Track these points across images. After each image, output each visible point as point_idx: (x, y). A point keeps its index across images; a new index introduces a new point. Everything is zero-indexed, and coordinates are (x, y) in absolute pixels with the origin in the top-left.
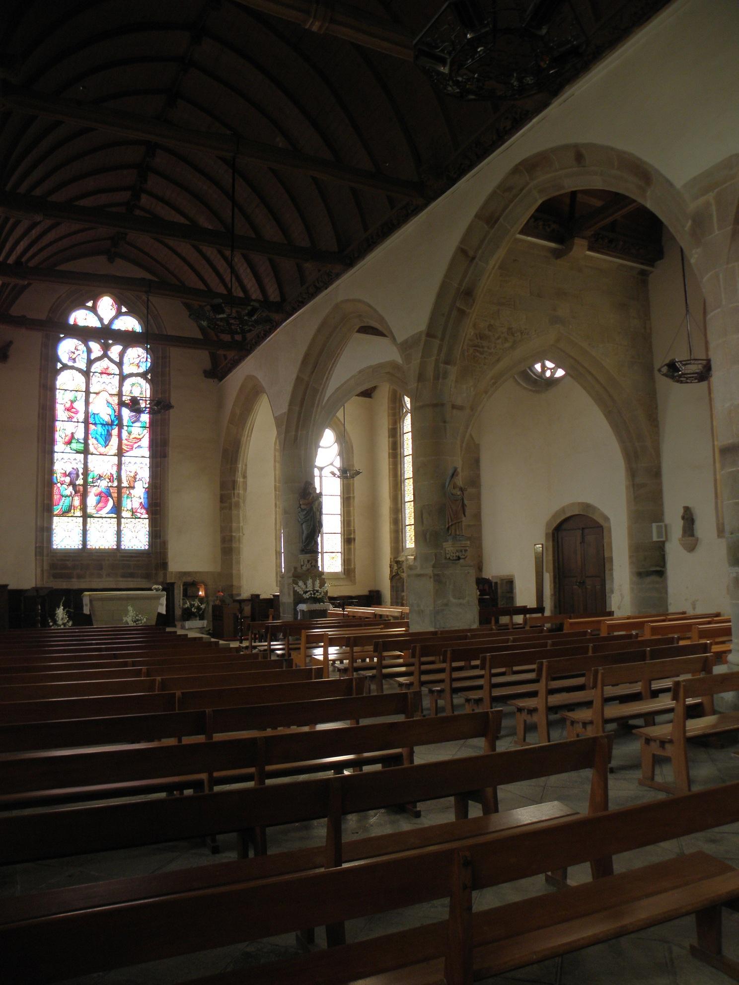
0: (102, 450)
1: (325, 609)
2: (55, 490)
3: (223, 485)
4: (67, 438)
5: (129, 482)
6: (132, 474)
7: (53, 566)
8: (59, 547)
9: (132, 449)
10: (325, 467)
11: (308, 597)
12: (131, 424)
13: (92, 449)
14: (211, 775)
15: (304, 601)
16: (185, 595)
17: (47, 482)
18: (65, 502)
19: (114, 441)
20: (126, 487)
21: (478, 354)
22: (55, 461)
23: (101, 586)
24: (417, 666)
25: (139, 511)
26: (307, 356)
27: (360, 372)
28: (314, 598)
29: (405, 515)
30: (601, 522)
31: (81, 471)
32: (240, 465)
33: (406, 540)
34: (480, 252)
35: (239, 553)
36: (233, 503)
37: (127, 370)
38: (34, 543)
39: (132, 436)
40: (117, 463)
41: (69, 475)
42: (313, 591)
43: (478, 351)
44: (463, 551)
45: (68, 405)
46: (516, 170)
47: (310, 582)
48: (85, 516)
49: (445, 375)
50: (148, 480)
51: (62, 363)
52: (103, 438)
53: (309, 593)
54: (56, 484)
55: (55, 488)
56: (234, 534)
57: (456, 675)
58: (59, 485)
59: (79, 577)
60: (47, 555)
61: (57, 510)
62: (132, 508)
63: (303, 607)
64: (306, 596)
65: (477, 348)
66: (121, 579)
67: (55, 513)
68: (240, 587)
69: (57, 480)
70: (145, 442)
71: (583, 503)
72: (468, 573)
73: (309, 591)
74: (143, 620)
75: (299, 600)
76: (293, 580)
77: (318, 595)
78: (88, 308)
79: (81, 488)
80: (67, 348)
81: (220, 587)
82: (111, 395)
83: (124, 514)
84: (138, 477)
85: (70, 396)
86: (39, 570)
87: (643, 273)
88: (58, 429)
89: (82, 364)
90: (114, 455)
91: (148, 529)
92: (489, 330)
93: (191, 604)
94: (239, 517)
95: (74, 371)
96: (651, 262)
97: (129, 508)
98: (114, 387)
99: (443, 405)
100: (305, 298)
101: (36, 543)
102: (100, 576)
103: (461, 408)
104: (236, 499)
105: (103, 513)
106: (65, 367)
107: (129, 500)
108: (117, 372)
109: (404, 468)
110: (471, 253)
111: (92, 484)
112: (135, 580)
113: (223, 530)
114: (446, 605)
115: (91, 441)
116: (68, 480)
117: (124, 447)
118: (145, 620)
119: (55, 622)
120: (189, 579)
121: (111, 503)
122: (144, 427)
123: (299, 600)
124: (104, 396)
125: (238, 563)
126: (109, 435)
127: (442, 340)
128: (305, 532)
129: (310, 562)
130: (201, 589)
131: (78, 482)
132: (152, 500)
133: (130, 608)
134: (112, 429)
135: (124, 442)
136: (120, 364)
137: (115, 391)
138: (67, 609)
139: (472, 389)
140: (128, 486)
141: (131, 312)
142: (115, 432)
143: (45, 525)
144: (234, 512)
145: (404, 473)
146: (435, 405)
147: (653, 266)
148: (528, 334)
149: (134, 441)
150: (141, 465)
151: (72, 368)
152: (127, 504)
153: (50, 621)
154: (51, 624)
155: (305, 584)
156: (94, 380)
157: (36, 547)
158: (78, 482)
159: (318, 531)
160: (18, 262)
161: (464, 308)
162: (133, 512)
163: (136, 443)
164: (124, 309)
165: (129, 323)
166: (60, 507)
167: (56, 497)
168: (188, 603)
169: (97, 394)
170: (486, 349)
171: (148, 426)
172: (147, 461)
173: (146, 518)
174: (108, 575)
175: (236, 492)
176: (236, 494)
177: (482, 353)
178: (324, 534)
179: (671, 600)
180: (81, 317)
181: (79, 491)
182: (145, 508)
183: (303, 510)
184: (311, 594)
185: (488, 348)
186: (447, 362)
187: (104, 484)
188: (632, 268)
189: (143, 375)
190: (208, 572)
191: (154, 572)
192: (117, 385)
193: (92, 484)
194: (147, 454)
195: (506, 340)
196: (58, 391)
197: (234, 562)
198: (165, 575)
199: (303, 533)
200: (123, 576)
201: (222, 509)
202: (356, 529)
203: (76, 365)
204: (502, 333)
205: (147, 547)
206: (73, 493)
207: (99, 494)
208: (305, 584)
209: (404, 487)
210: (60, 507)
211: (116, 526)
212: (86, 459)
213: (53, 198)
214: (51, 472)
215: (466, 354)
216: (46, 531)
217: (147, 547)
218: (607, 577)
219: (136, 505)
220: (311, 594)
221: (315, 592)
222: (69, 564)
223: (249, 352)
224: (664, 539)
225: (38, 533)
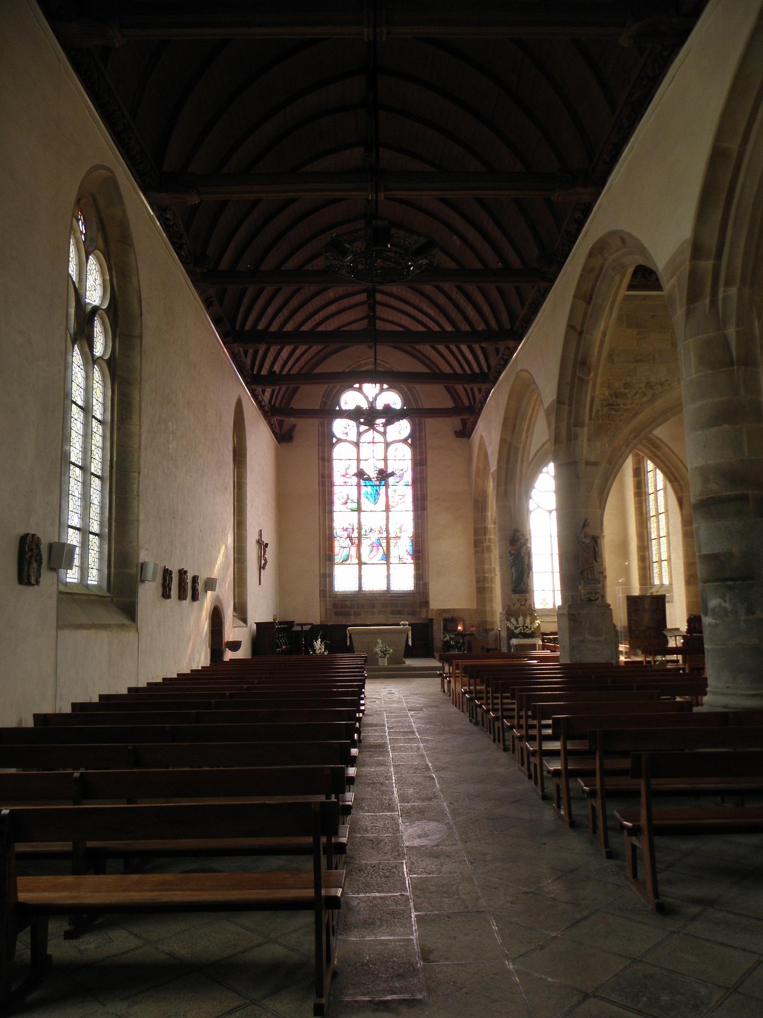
0: (373, 507)
3: (476, 532)
7: (335, 606)
11: (518, 632)
12: (396, 484)
13: (363, 508)
15: (516, 636)
16: (446, 629)
17: (328, 538)
21: (613, 412)
28: (524, 633)
29: (652, 552)
31: (356, 526)
32: (489, 513)
33: (654, 577)
34: (585, 326)
35: (492, 591)
38: (318, 586)
41: (346, 530)
42: (523, 627)
43: (612, 409)
44: (593, 593)
46: (591, 255)
47: (521, 619)
48: (360, 563)
53: (519, 629)
56: (486, 575)
57: (505, 701)
60: (330, 597)
61: (337, 559)
63: (514, 641)
64: (517, 631)
73: (519, 627)
74: (390, 650)
75: (511, 635)
76: (506, 618)
78: (356, 389)
79: (357, 541)
80: (341, 427)
81: (476, 622)
86: (323, 610)
92: (625, 388)
93: (450, 638)
95: (347, 444)
100: (500, 369)
101: (320, 587)
102: (373, 613)
104: (488, 544)
106: (339, 440)
107: (396, 547)
109: (649, 505)
110: (578, 328)
111: (365, 536)
112: (402, 616)
114: (582, 641)
116: (345, 534)
118: (391, 650)
119: (314, 651)
120: (448, 616)
123: (511, 635)
124: (372, 461)
127: (570, 405)
129: (520, 601)
130: (459, 625)
132: (416, 548)
133: (379, 641)
136: (384, 434)
139: (607, 445)
144: (486, 555)
145: (649, 511)
148: (669, 385)
151: (345, 441)
154: (311, 653)
155: (517, 620)
156: (363, 447)
157: (320, 591)
159: (527, 573)
160: (271, 372)
161: (583, 377)
165: (392, 399)
168: (448, 637)
170: (622, 406)
174: (380, 612)
175: (487, 537)
176: (487, 539)
177: (617, 411)
183: (512, 555)
184: (521, 630)
186: (576, 425)
189: (405, 441)
190: (464, 609)
193: (365, 536)
195: (644, 394)
198: (427, 612)
199: (513, 576)
200: (393, 613)
201: (476, 552)
203: (349, 438)
206: (350, 544)
207: (372, 545)
208: (517, 620)
209: (650, 525)
214: (331, 528)
215: (600, 413)
216: (327, 577)
217: (412, 588)
220: (521, 630)
221: (525, 627)
222: (348, 603)
223: (479, 414)
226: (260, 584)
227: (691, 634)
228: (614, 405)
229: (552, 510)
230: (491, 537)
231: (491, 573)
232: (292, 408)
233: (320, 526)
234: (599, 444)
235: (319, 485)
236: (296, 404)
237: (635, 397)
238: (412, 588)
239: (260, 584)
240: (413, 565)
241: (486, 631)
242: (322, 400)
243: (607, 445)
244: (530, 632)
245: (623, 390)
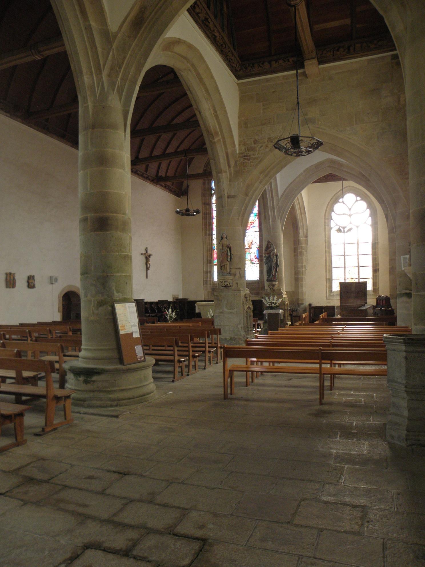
1: (278, 313)
5: (249, 245)
6: (250, 241)
14: (19, 373)
20: (248, 248)
21: (246, 161)
22: (214, 239)
24: (190, 345)
25: (254, 260)
27: (305, 171)
36: (298, 252)
38: (203, 279)
44: (223, 282)
47: (271, 298)
54: (214, 250)
55: (214, 252)
56: (299, 270)
60: (210, 284)
62: (251, 259)
65: (246, 157)
67: (215, 264)
68: (303, 300)
69: (215, 248)
72: (237, 294)
77: (273, 305)
84: (253, 242)
86: (206, 292)
92: (255, 144)
94: (302, 261)
97: (249, 259)
101: (204, 279)
104: (301, 250)
107: (249, 255)
114: (222, 313)
122: (256, 216)
125: (302, 286)
138: (176, 310)
140: (248, 247)
143: (209, 270)
144: (299, 257)
149: (251, 224)
155: (269, 298)
162: (251, 261)
163: (252, 225)
171: (257, 215)
172: (258, 233)
173: (257, 264)
175: (301, 246)
177: (248, 160)
178: (360, 267)
182: (257, 258)
184: (269, 304)
185: (253, 155)
188: (383, 58)
195: (267, 146)
197: (299, 286)
201: (295, 256)
208: (269, 298)
215: (238, 163)
217: (258, 279)
220: (269, 304)
225: (204, 274)
226: (147, 277)
227: (375, 309)
228: (247, 156)
229: (338, 225)
230: (303, 246)
231: (302, 268)
232: (168, 176)
233: (203, 243)
234: (236, 183)
235: (202, 219)
236: (190, 172)
237: (261, 149)
238: (258, 279)
239: (147, 277)
240: (259, 264)
241: (299, 305)
242: (204, 169)
243: (241, 183)
244: (275, 306)
245: (253, 145)
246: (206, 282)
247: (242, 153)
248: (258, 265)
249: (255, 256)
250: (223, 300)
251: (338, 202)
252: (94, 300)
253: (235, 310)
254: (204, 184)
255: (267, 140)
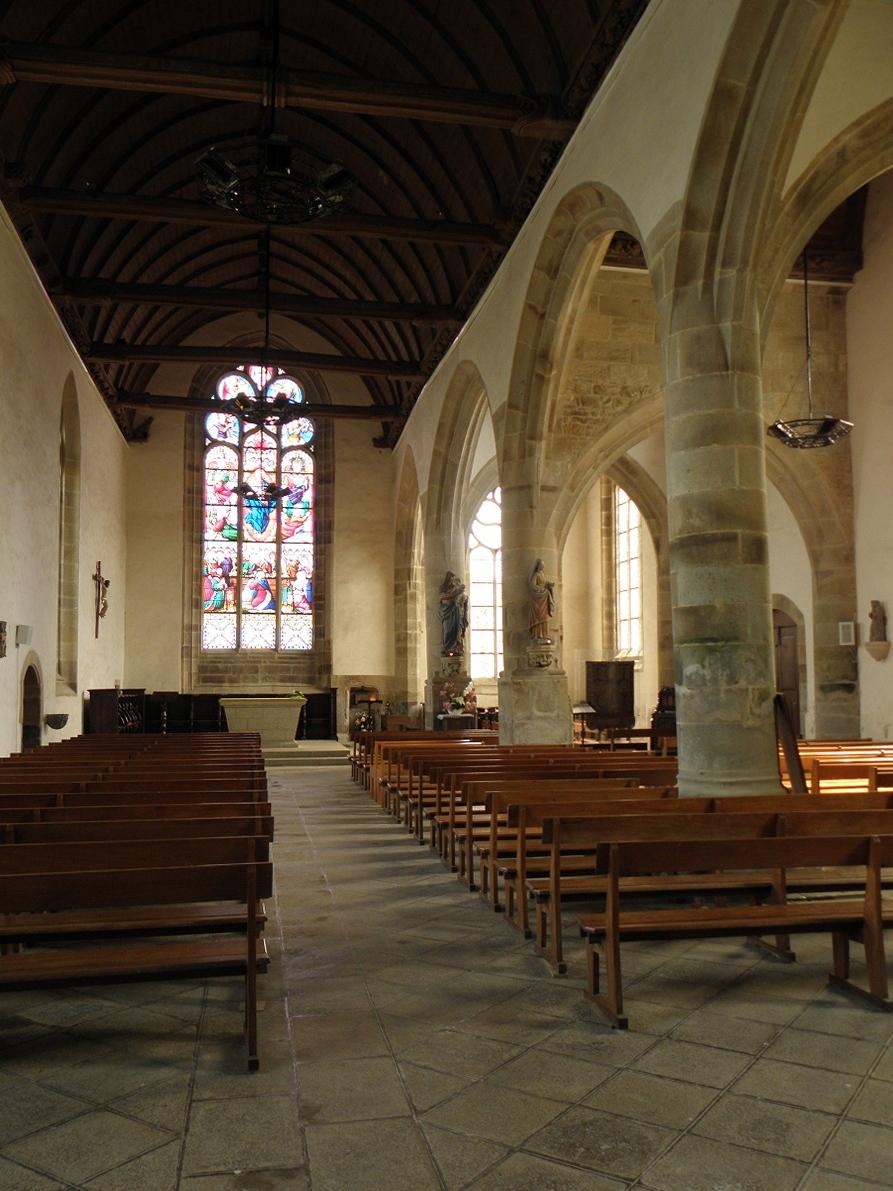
0: (259, 536)
2: (206, 584)
4: (219, 524)
6: (293, 564)
7: (202, 669)
8: (210, 648)
9: (293, 534)
10: (490, 549)
13: (246, 536)
18: (219, 596)
19: (272, 525)
21: (579, 423)
23: (255, 692)
25: (301, 605)
26: (441, 426)
30: (796, 619)
31: (235, 561)
37: (286, 442)
39: (293, 519)
40: (275, 551)
41: (221, 566)
45: (219, 486)
49: (531, 452)
50: (311, 569)
51: (210, 439)
52: (260, 522)
58: (210, 577)
59: (231, 681)
60: (196, 657)
66: (279, 684)
70: (308, 526)
71: (778, 595)
72: (558, 682)
78: (239, 373)
79: (235, 580)
80: (214, 422)
82: (268, 472)
83: (284, 609)
85: (220, 476)
86: (186, 673)
87: (835, 291)
88: (208, 514)
89: (234, 440)
90: (273, 542)
91: (311, 626)
92: (595, 393)
96: (848, 276)
97: (290, 603)
98: (271, 463)
99: (529, 487)
101: (183, 643)
103: (553, 489)
104: (412, 590)
105: (261, 608)
106: (215, 443)
107: (290, 593)
108: (274, 445)
110: (540, 310)
112: (295, 685)
113: (397, 627)
115: (246, 526)
116: (220, 571)
117: (284, 532)
120: (357, 685)
121: (269, 597)
126: (266, 518)
128: (446, 632)
131: (231, 574)
134: (270, 512)
135: (284, 526)
136: (277, 437)
137: (272, 468)
139: (569, 465)
141: (289, 375)
142: (273, 515)
143: (194, 623)
146: (521, 488)
147: (850, 280)
148: (650, 392)
149: (296, 524)
150: (304, 553)
151: (223, 443)
152: (287, 598)
153: (781, 749)
158: (231, 574)
162: (294, 606)
164: (281, 372)
165: (289, 388)
166: (211, 602)
167: (206, 591)
169: (252, 472)
170: (590, 416)
172: (311, 548)
174: (265, 679)
175: (413, 581)
177: (583, 421)
179: (864, 723)
180: (232, 386)
181: (233, 584)
183: (442, 605)
185: (593, 414)
187: (260, 576)
189: (305, 448)
191: (317, 676)
192: (275, 461)
194: (310, 539)
195: (619, 402)
196: (207, 471)
197: (409, 665)
200: (282, 680)
201: (396, 602)
202: (564, 624)
203: (227, 440)
204: (613, 394)
205: (310, 647)
207: (256, 588)
210: (211, 602)
211: (274, 623)
212: (240, 547)
213: (145, 279)
214: (200, 563)
215: (563, 424)
216: (194, 630)
217: (310, 647)
218: (801, 692)
219: (298, 599)
224: (852, 643)
226: (97, 637)
233: (184, 560)
234: (559, 464)
236: (154, 388)
237: (607, 405)
239: (97, 637)
245: (592, 395)
246: (187, 652)
247: (570, 407)
248: (310, 617)
249: (304, 597)
250: (531, 693)
251: (485, 499)
252: (753, 689)
253: (556, 712)
254: (189, 419)
255: (619, 390)
